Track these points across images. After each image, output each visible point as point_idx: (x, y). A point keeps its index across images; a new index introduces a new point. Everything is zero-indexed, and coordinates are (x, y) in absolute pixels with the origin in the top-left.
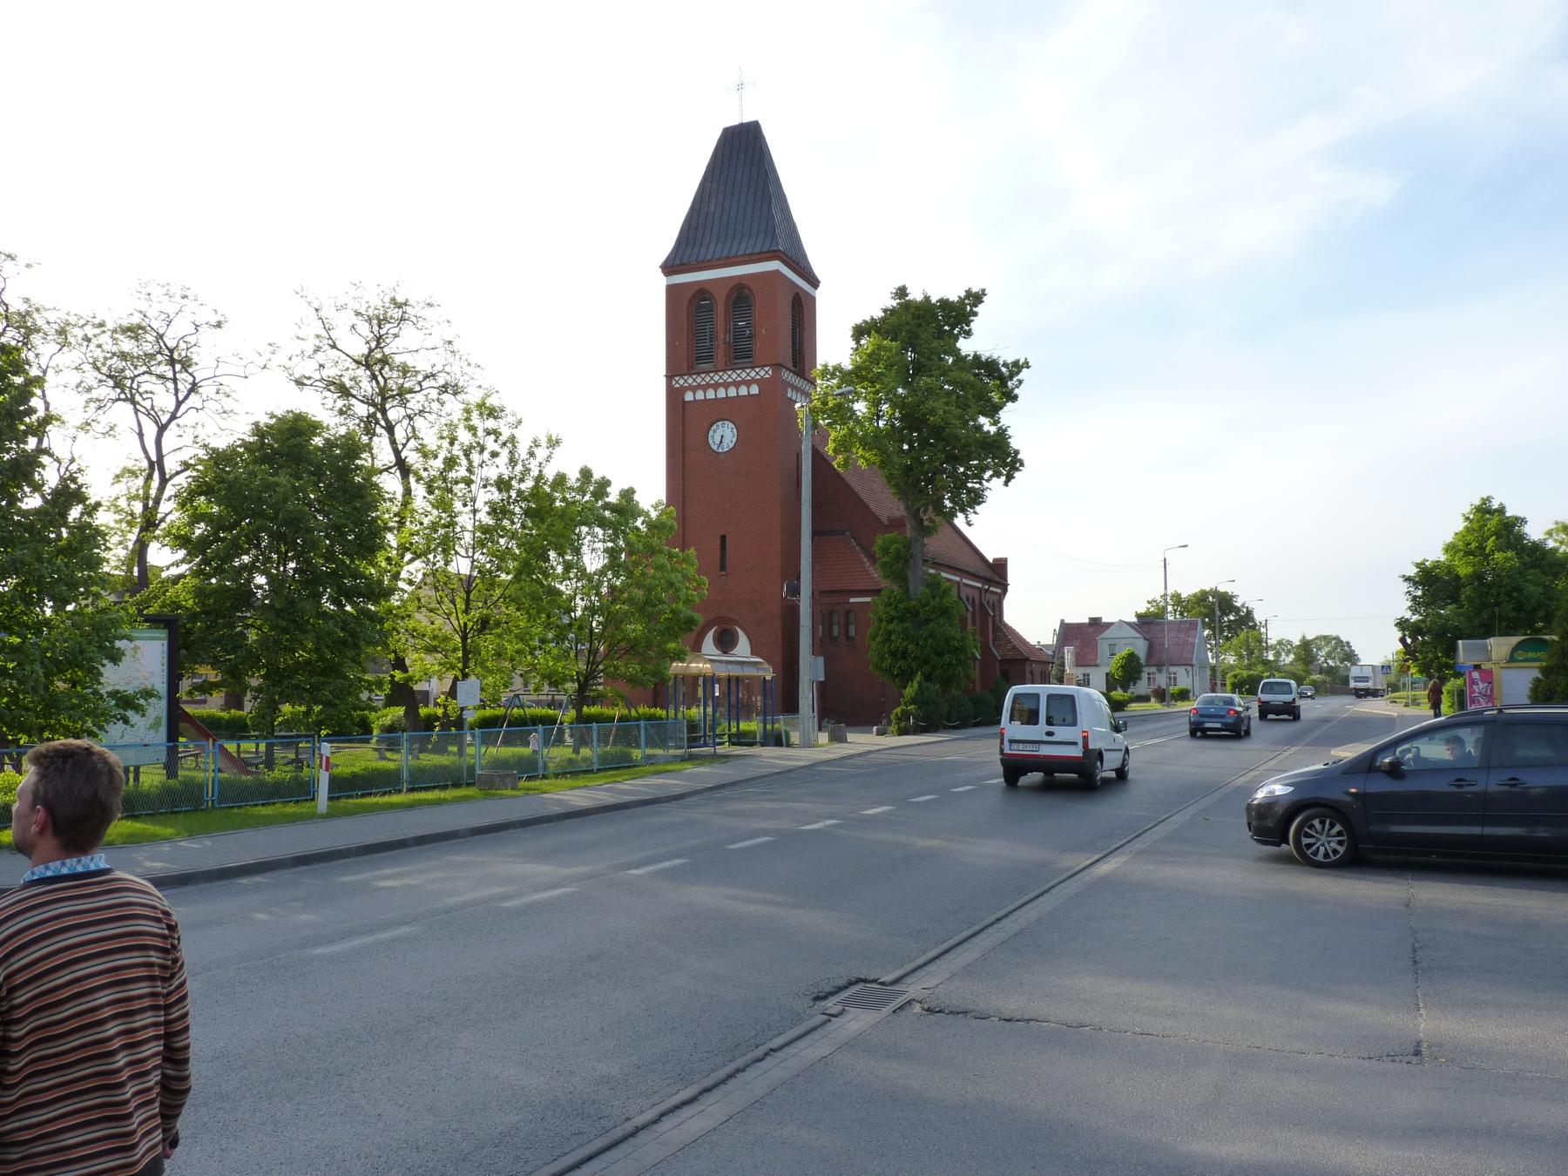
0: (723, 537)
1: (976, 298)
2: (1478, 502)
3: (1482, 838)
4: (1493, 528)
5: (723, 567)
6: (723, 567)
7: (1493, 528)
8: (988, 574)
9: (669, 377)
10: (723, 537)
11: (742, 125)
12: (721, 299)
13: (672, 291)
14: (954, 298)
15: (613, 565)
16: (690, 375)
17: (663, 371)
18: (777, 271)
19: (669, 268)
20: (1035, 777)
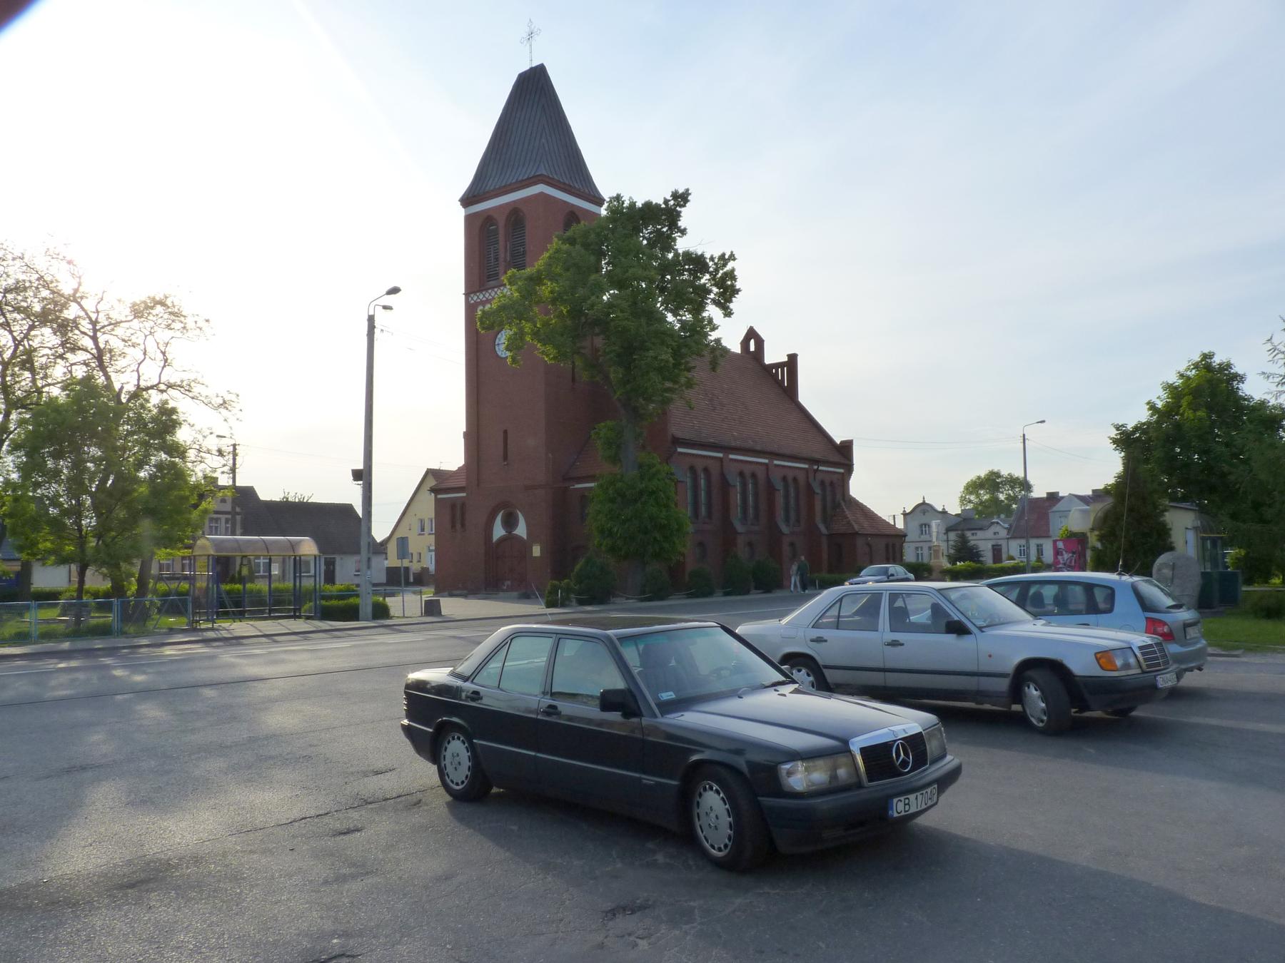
0: (505, 432)
1: (682, 198)
2: (1197, 358)
3: (519, 747)
4: (1210, 389)
5: (505, 458)
6: (505, 458)
7: (1210, 389)
8: (837, 458)
9: (467, 294)
10: (505, 432)
11: (531, 69)
12: (501, 223)
13: (469, 220)
14: (658, 200)
15: (1170, 475)
16: (481, 291)
17: (463, 291)
18: (542, 194)
19: (467, 201)
20: (1160, 629)
